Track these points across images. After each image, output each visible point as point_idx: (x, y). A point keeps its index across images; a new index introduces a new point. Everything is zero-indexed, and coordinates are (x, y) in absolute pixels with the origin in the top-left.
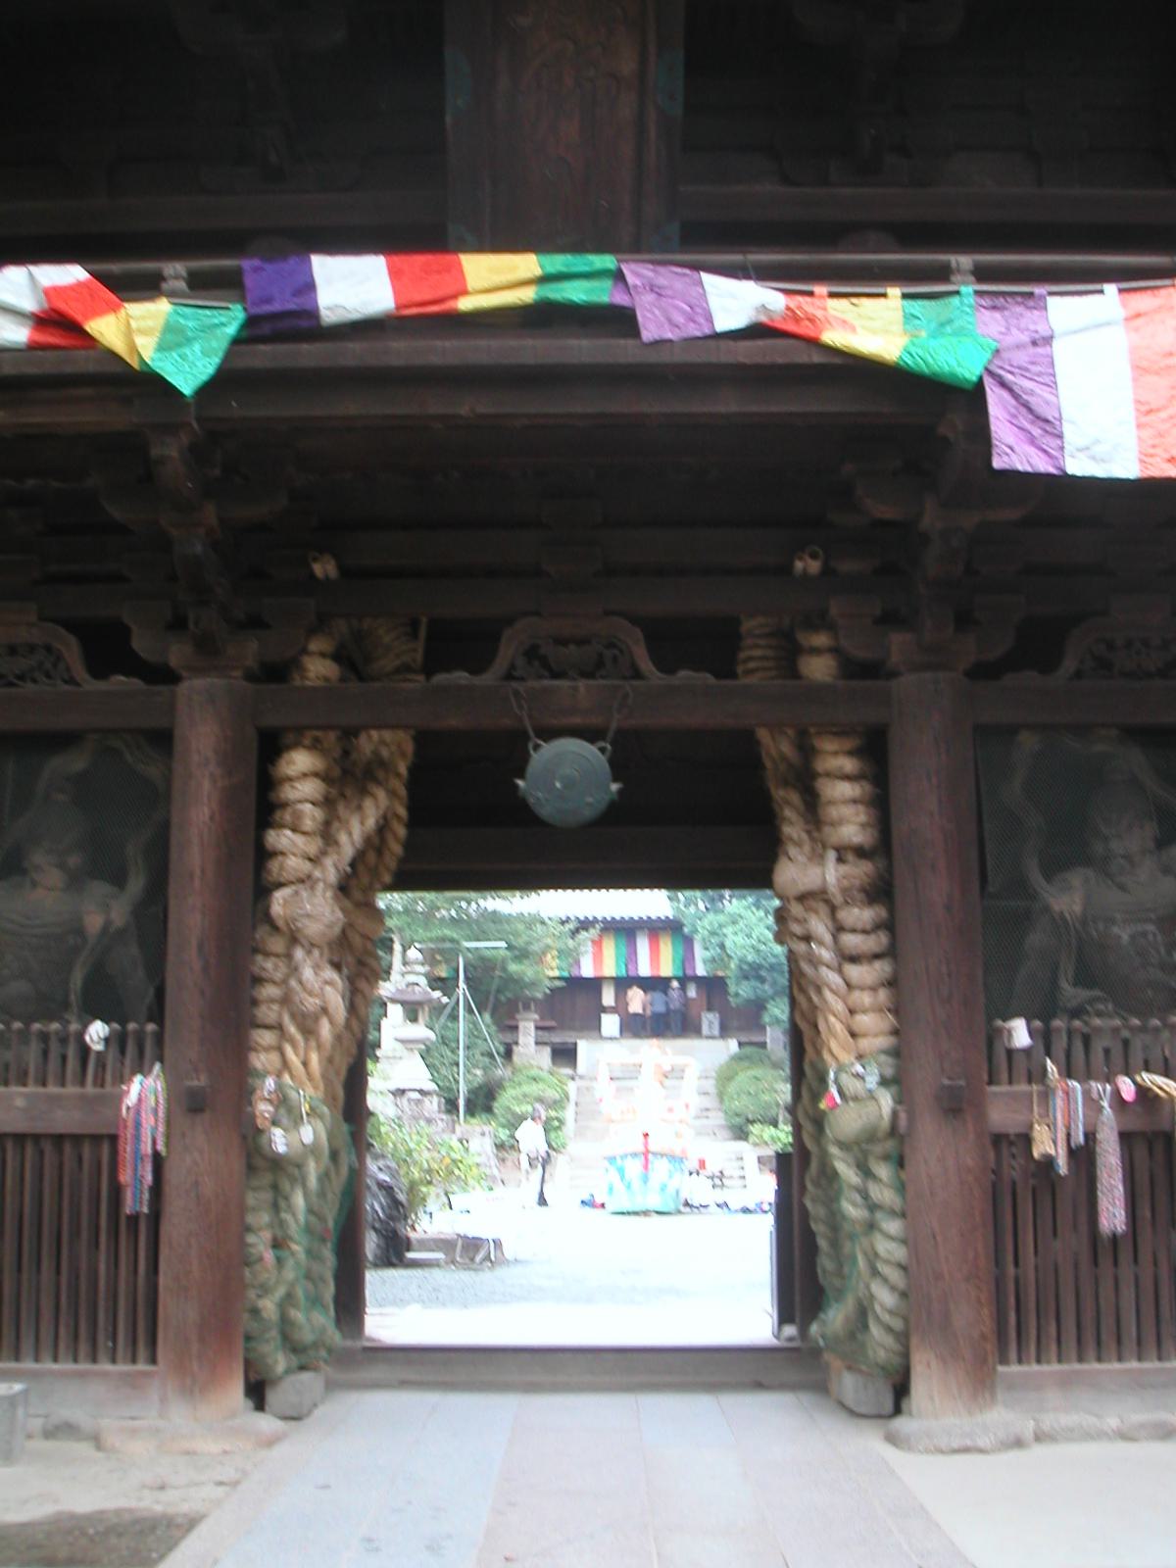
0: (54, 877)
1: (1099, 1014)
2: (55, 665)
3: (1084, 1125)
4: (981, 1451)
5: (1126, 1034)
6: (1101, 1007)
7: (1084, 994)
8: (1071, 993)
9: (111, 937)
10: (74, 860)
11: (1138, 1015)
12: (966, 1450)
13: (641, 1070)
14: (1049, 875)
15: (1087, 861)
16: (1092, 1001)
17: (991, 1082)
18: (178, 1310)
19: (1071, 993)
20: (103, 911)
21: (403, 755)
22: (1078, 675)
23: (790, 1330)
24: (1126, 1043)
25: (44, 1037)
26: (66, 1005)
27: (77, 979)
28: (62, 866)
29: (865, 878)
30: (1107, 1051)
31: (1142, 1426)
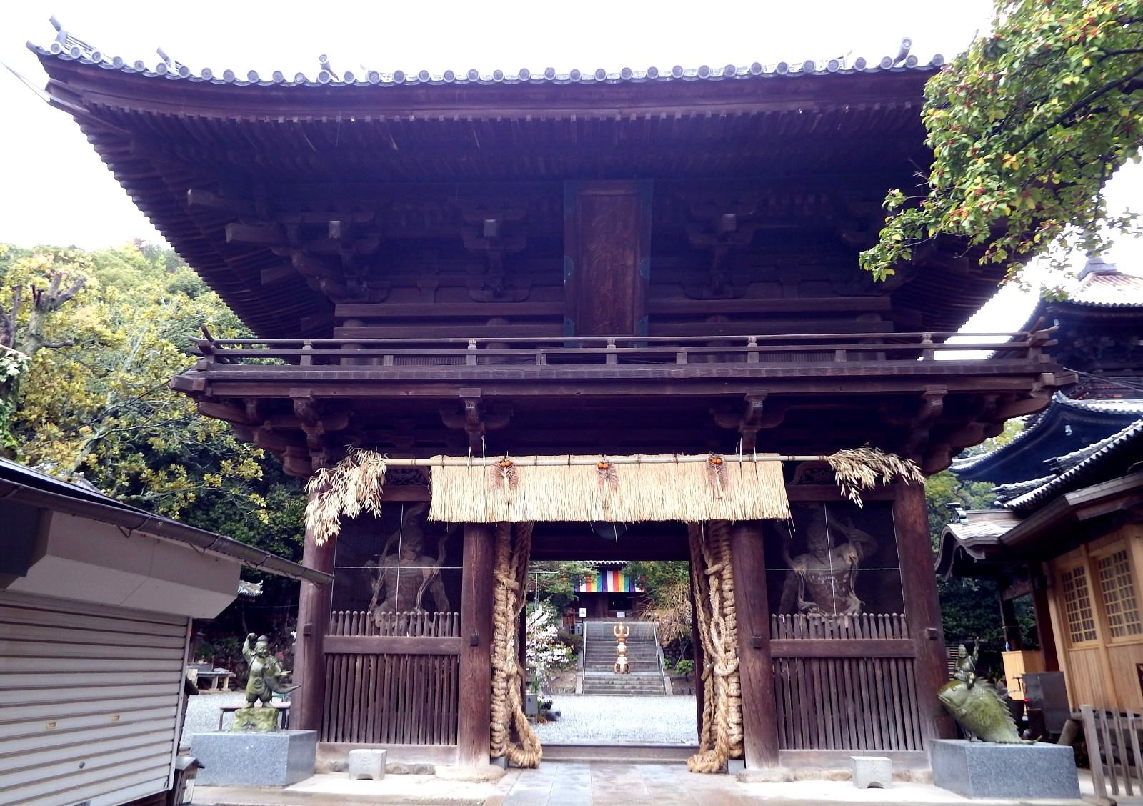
0: (410, 554)
1: (814, 612)
2: (420, 477)
3: (1065, 745)
4: (773, 782)
5: (823, 620)
6: (815, 609)
7: (807, 604)
8: (803, 604)
9: (434, 579)
10: (418, 549)
11: (827, 611)
12: (767, 781)
13: (1140, 609)
14: (792, 558)
15: (807, 551)
16: (811, 607)
17: (771, 638)
18: (466, 724)
19: (803, 604)
20: (429, 569)
21: (191, 293)
22: (800, 482)
23: (924, 144)
24: (824, 623)
25: (408, 618)
27: (420, 594)
28: (414, 551)
29: (770, 764)
30: (816, 626)
31: (837, 775)
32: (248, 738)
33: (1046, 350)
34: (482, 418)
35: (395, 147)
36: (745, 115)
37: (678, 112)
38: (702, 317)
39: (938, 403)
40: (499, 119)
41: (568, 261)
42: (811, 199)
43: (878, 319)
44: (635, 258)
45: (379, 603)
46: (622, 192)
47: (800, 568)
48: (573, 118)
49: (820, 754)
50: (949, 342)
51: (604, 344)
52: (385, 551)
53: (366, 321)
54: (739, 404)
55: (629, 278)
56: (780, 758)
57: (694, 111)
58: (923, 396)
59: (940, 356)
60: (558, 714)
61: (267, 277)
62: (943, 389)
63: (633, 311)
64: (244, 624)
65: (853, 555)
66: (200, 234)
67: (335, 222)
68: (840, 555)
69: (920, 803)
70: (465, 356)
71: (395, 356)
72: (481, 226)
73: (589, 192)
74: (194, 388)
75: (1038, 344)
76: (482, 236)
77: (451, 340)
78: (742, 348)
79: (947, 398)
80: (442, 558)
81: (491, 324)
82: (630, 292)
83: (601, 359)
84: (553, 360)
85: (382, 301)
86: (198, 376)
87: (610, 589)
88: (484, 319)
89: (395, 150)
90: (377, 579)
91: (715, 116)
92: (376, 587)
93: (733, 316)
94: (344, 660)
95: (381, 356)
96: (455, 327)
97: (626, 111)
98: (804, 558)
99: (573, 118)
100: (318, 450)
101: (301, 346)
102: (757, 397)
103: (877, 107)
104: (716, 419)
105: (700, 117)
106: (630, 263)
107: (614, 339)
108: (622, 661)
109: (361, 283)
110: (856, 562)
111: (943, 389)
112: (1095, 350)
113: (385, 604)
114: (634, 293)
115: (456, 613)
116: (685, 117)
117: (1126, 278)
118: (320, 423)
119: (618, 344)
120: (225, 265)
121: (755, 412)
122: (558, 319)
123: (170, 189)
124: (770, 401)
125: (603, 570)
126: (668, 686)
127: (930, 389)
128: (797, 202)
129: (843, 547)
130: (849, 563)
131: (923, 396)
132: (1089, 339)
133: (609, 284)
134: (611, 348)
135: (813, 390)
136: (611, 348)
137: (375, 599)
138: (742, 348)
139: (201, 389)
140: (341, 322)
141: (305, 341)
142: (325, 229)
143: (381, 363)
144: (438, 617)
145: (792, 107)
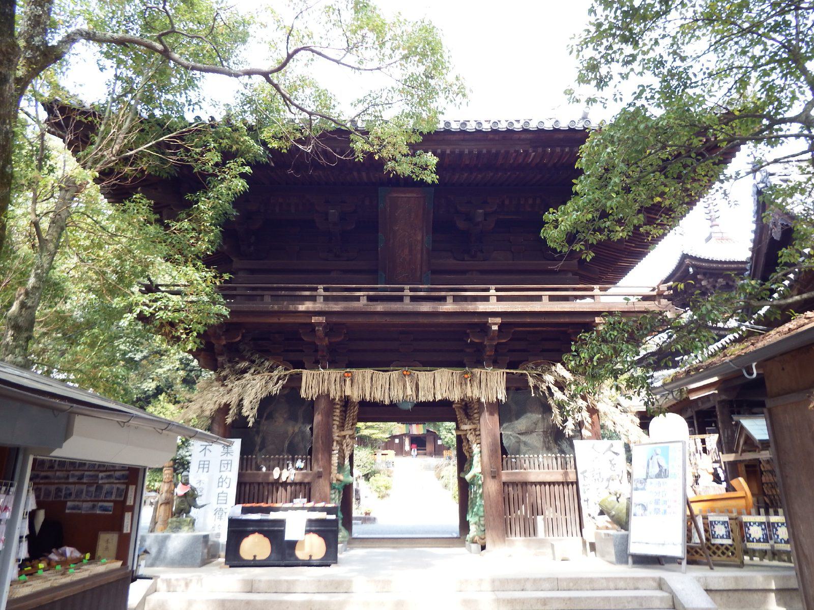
10: (285, 416)
26: (283, 451)
27: (286, 445)
33: (665, 297)
34: (326, 335)
35: (273, 164)
38: (464, 272)
39: (495, 328)
41: (381, 236)
43: (570, 275)
44: (423, 236)
45: (260, 450)
49: (530, 540)
50: (609, 292)
51: (402, 290)
53: (252, 271)
55: (419, 248)
56: (507, 543)
59: (604, 299)
60: (375, 519)
62: (499, 320)
63: (421, 268)
69: (648, 568)
70: (316, 296)
71: (272, 296)
73: (395, 195)
75: (660, 295)
78: (314, 293)
82: (419, 256)
83: (400, 299)
84: (370, 299)
88: (328, 272)
90: (259, 435)
92: (258, 440)
93: (483, 272)
94: (257, 487)
95: (262, 296)
96: (485, 277)
100: (221, 354)
101: (316, 289)
103: (567, 150)
105: (461, 154)
106: (419, 238)
107: (408, 286)
112: (714, 287)
113: (264, 451)
114: (422, 258)
115: (572, 455)
118: (223, 337)
119: (325, 290)
124: (501, 326)
127: (490, 320)
128: (522, 202)
132: (711, 280)
133: (406, 251)
134: (407, 293)
136: (321, 291)
137: (257, 448)
138: (314, 293)
141: (595, 286)
143: (262, 300)
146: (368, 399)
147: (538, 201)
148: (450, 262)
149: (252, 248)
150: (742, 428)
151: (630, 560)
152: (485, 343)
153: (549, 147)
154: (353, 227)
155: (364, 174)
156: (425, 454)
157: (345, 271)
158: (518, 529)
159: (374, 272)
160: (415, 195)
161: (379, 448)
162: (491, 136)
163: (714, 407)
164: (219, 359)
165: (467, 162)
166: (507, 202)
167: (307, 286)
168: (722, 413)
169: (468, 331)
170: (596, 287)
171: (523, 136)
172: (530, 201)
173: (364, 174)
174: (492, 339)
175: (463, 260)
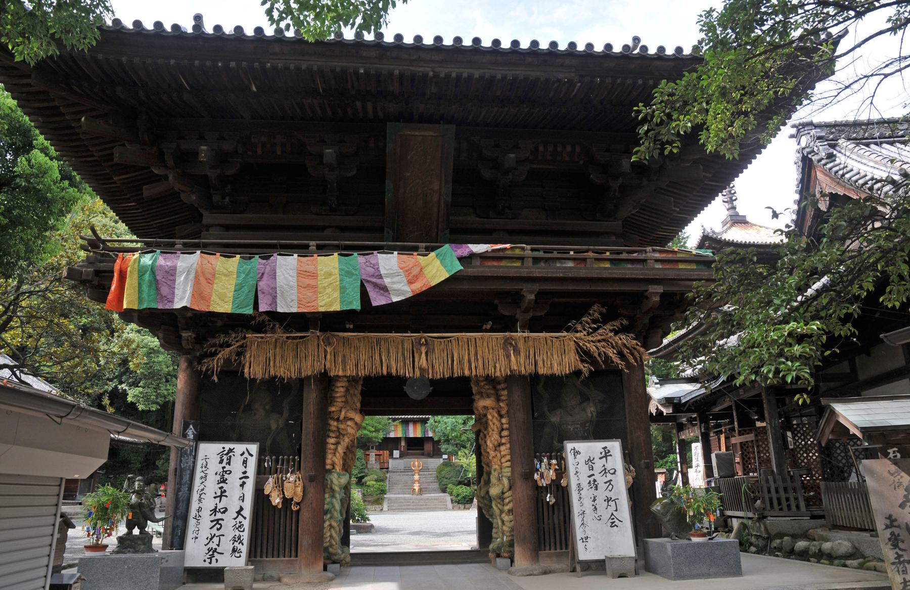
10: (267, 407)
18: (305, 541)
32: (127, 559)
35: (254, 89)
36: (526, 79)
37: (477, 74)
40: (338, 70)
41: (389, 185)
42: (569, 148)
43: (613, 238)
46: (431, 133)
47: (555, 419)
48: (397, 72)
52: (241, 410)
53: (228, 228)
54: (515, 298)
57: (488, 73)
58: (646, 294)
61: (148, 191)
62: (660, 289)
64: (479, 248)
65: (592, 409)
66: (93, 156)
67: (204, 148)
68: (584, 410)
72: (321, 156)
74: (84, 277)
76: (321, 163)
77: (296, 242)
79: (663, 295)
80: (286, 413)
81: (327, 232)
85: (241, 213)
86: (87, 267)
87: (411, 435)
88: (323, 228)
89: (254, 92)
91: (504, 78)
97: (437, 70)
98: (558, 412)
99: (397, 72)
102: (531, 292)
103: (619, 81)
104: (500, 308)
105: (493, 79)
106: (436, 188)
107: (424, 244)
108: (416, 487)
109: (224, 198)
110: (594, 414)
111: (660, 289)
116: (482, 77)
117: (753, 225)
120: (115, 183)
121: (529, 302)
122: (380, 230)
123: (67, 117)
124: (540, 294)
125: (406, 422)
126: (450, 505)
128: (559, 149)
129: (585, 404)
130: (590, 415)
131: (646, 294)
135: (571, 287)
139: (90, 278)
140: (208, 227)
142: (196, 153)
144: (283, 461)
145: (560, 76)
146: (394, 374)
147: (578, 149)
148: (472, 220)
149: (227, 200)
150: (833, 412)
151: (578, 568)
152: (517, 316)
153: (599, 77)
154: (354, 172)
155: (369, 106)
156: (423, 454)
157: (343, 229)
158: (552, 540)
159: (380, 230)
160: (431, 133)
161: (372, 448)
162: (529, 60)
163: (760, 395)
164: (183, 335)
165: (498, 94)
166: (541, 148)
167: (296, 242)
168: (769, 402)
169: (496, 301)
170: (649, 249)
171: (568, 61)
172: (569, 148)
173: (369, 106)
174: (526, 311)
175: (488, 218)
